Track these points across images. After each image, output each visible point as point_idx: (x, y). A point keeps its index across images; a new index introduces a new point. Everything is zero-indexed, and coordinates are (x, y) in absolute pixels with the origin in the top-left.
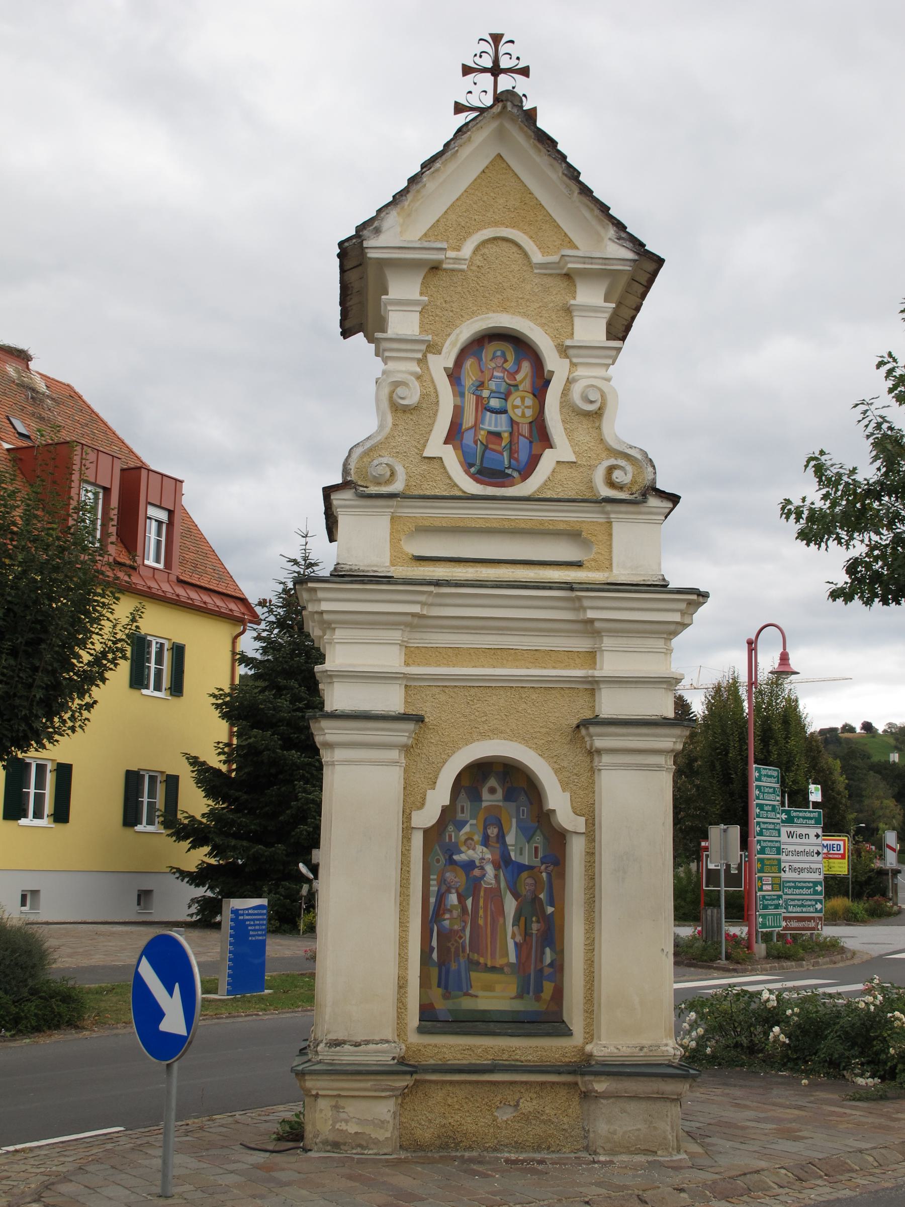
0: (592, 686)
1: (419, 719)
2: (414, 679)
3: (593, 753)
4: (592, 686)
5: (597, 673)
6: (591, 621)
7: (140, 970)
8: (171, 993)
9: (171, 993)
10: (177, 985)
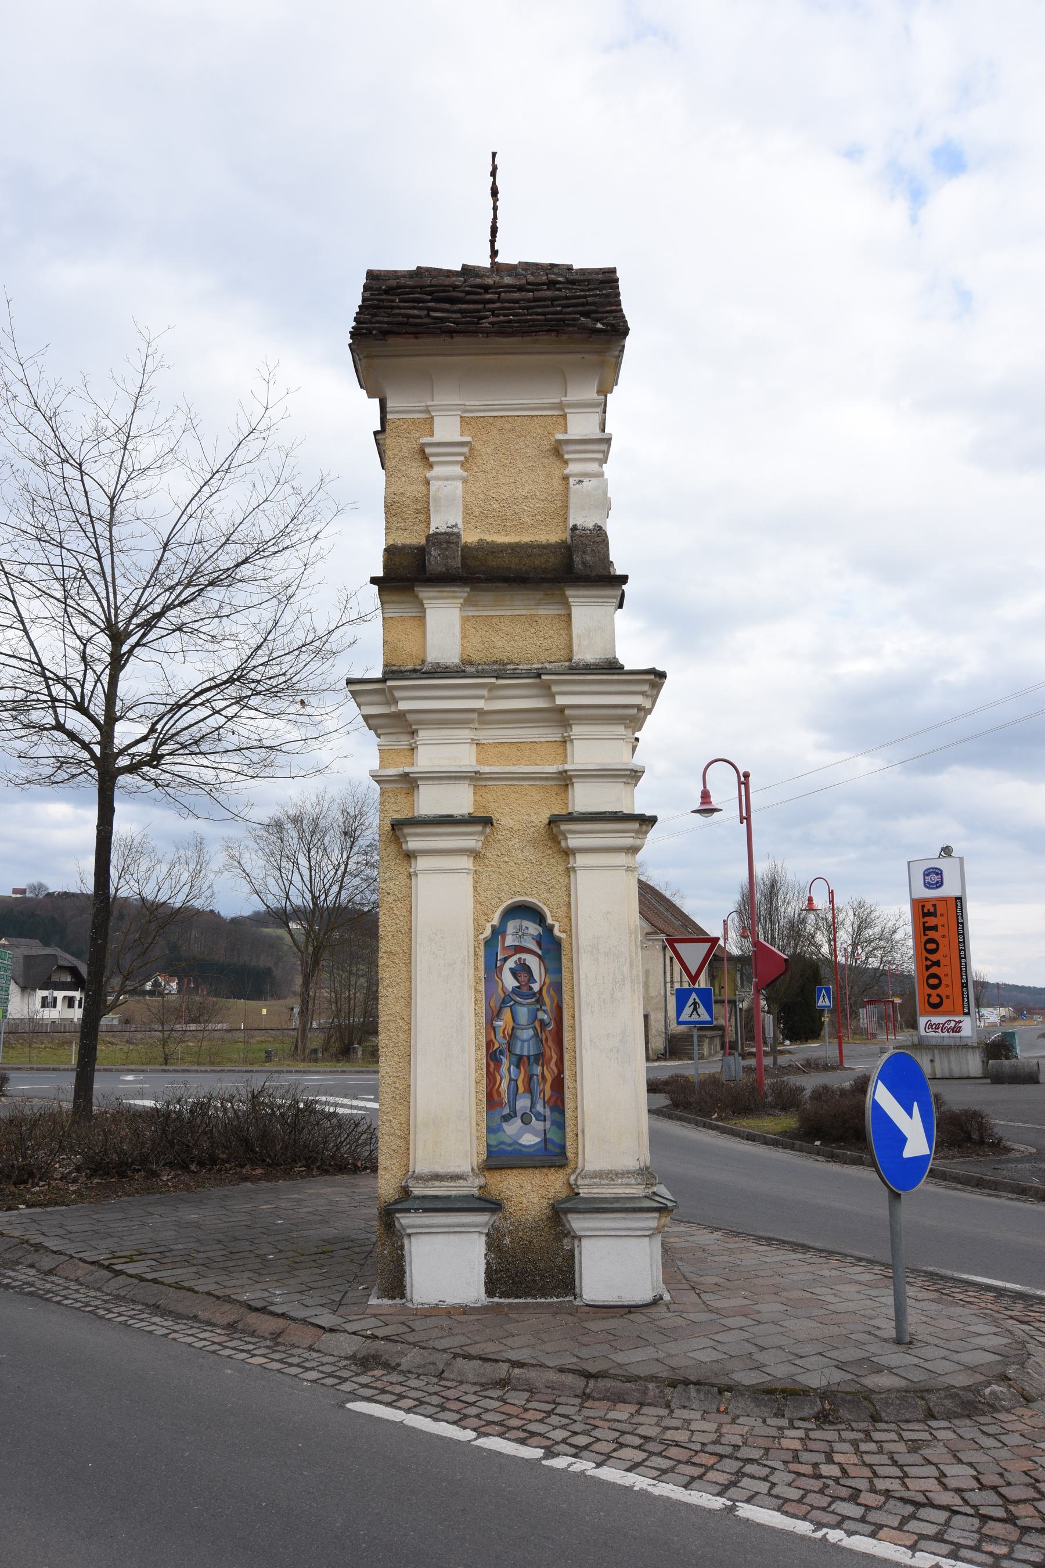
0: (565, 780)
1: (487, 822)
2: (490, 779)
3: (568, 853)
4: (565, 780)
5: (567, 767)
6: (561, 709)
7: (876, 1098)
8: (911, 1115)
9: (911, 1115)
10: (915, 1104)
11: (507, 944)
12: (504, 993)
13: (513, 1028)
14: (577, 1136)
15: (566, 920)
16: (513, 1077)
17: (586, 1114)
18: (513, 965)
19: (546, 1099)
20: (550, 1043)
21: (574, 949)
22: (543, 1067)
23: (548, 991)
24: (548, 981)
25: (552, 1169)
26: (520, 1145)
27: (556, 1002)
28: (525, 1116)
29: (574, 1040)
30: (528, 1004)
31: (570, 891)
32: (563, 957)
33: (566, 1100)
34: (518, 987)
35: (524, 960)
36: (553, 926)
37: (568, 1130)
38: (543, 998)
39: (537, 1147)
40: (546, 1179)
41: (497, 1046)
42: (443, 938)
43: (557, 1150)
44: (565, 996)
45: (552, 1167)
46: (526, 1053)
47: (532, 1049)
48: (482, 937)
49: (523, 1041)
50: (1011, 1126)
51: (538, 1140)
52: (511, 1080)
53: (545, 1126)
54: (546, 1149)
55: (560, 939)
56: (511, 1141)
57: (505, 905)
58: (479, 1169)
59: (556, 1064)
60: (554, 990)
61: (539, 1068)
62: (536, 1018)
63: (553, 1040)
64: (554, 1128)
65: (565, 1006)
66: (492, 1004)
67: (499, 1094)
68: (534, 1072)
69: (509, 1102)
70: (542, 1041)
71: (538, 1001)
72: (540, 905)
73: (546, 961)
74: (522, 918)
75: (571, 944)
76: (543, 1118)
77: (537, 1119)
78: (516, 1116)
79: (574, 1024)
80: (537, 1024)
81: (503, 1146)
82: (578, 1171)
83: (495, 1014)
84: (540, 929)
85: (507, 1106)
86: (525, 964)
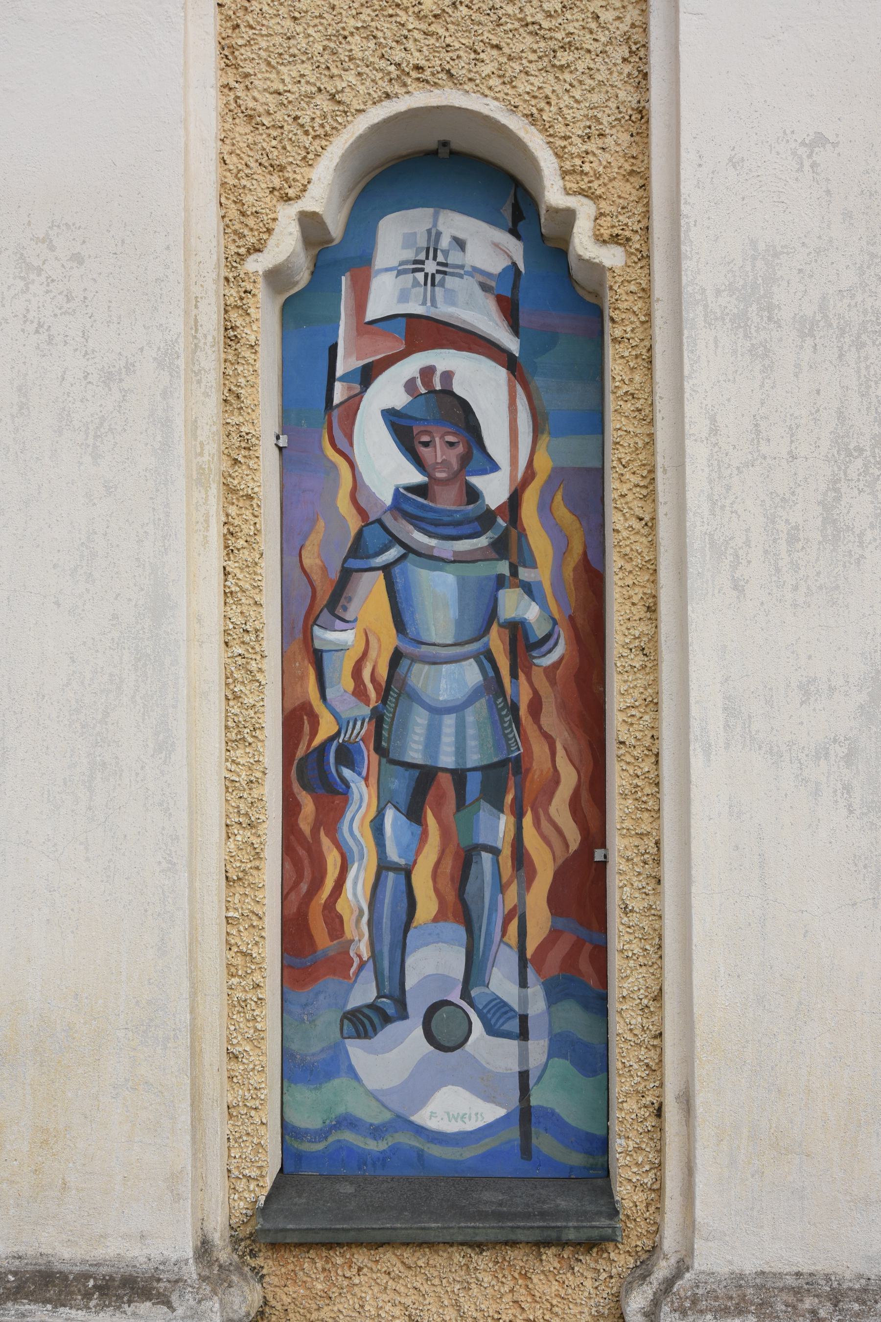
11: (375, 310)
12: (361, 512)
13: (397, 657)
14: (659, 1113)
15: (627, 189)
16: (393, 854)
17: (700, 1028)
18: (399, 400)
19: (531, 948)
20: (550, 719)
21: (660, 312)
22: (519, 815)
23: (545, 507)
24: (544, 464)
25: (549, 1254)
26: (420, 1131)
27: (577, 548)
28: (444, 1012)
29: (654, 705)
30: (459, 560)
31: (644, 60)
32: (610, 350)
33: (616, 963)
34: (420, 490)
35: (448, 376)
36: (568, 217)
37: (620, 1086)
38: (522, 534)
39: (488, 1144)
40: (522, 1295)
41: (327, 727)
42: (78, 259)
43: (576, 1159)
44: (614, 519)
45: (548, 1244)
46: (447, 760)
47: (472, 744)
48: (257, 265)
49: (437, 711)
50: (410, 499)
51: (492, 1113)
52: (384, 866)
53: (523, 1056)
54: (526, 1149)
55: (597, 269)
56: (382, 1117)
57: (360, 125)
58: (235, 1241)
59: (575, 804)
60: (569, 503)
61: (504, 823)
62: (492, 614)
63: (563, 708)
64: (561, 1065)
65: (614, 562)
66: (310, 560)
67: (335, 924)
68: (483, 838)
69: (375, 955)
70: (514, 709)
71: (500, 548)
72: (515, 124)
73: (538, 382)
74: (441, 203)
75: (646, 293)
76: (513, 1026)
77: (491, 1030)
78: (403, 1014)
79: (654, 638)
80: (497, 642)
81: (348, 1136)
82: (662, 1270)
83: (323, 597)
84: (516, 249)
85: (368, 974)
86: (448, 392)
